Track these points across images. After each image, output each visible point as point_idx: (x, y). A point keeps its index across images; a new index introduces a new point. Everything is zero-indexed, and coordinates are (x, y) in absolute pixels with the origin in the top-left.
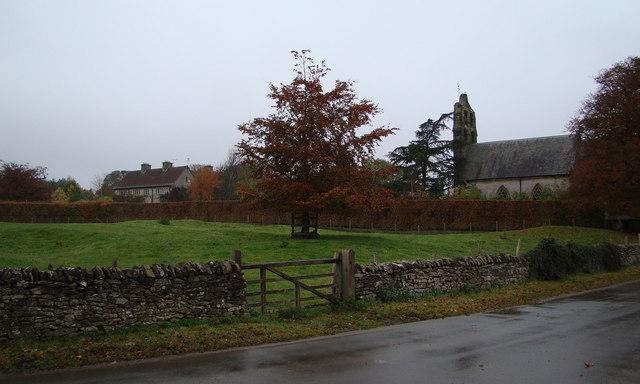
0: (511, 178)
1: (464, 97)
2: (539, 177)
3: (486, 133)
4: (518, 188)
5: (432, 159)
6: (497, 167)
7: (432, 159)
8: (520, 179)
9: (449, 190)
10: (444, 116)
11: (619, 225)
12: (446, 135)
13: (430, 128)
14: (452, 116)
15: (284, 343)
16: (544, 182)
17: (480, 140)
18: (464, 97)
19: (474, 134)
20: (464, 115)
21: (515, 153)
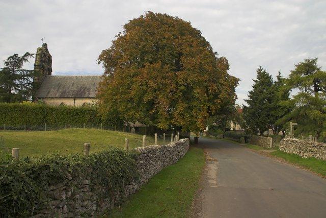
0: (69, 98)
1: (316, 59)
2: (86, 98)
3: (58, 69)
4: (73, 105)
5: (17, 82)
6: (60, 91)
7: (17, 82)
8: (75, 99)
9: (29, 102)
10: (27, 54)
11: (133, 129)
12: (29, 65)
13: (15, 61)
14: (35, 56)
15: (292, 166)
16: (88, 101)
17: (53, 74)
18: (45, 45)
19: (50, 70)
20: (44, 58)
21: (73, 84)
